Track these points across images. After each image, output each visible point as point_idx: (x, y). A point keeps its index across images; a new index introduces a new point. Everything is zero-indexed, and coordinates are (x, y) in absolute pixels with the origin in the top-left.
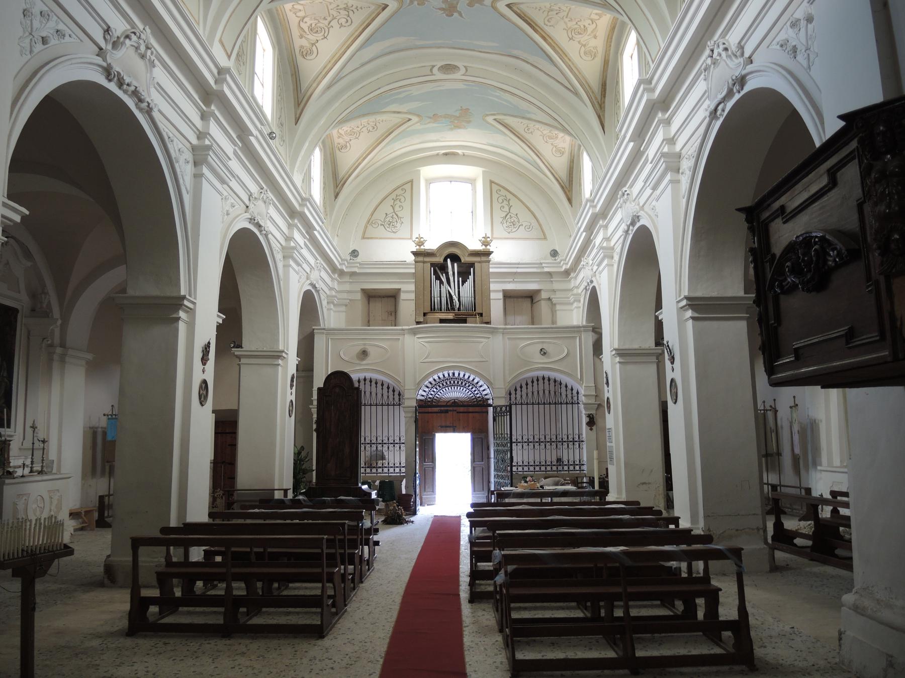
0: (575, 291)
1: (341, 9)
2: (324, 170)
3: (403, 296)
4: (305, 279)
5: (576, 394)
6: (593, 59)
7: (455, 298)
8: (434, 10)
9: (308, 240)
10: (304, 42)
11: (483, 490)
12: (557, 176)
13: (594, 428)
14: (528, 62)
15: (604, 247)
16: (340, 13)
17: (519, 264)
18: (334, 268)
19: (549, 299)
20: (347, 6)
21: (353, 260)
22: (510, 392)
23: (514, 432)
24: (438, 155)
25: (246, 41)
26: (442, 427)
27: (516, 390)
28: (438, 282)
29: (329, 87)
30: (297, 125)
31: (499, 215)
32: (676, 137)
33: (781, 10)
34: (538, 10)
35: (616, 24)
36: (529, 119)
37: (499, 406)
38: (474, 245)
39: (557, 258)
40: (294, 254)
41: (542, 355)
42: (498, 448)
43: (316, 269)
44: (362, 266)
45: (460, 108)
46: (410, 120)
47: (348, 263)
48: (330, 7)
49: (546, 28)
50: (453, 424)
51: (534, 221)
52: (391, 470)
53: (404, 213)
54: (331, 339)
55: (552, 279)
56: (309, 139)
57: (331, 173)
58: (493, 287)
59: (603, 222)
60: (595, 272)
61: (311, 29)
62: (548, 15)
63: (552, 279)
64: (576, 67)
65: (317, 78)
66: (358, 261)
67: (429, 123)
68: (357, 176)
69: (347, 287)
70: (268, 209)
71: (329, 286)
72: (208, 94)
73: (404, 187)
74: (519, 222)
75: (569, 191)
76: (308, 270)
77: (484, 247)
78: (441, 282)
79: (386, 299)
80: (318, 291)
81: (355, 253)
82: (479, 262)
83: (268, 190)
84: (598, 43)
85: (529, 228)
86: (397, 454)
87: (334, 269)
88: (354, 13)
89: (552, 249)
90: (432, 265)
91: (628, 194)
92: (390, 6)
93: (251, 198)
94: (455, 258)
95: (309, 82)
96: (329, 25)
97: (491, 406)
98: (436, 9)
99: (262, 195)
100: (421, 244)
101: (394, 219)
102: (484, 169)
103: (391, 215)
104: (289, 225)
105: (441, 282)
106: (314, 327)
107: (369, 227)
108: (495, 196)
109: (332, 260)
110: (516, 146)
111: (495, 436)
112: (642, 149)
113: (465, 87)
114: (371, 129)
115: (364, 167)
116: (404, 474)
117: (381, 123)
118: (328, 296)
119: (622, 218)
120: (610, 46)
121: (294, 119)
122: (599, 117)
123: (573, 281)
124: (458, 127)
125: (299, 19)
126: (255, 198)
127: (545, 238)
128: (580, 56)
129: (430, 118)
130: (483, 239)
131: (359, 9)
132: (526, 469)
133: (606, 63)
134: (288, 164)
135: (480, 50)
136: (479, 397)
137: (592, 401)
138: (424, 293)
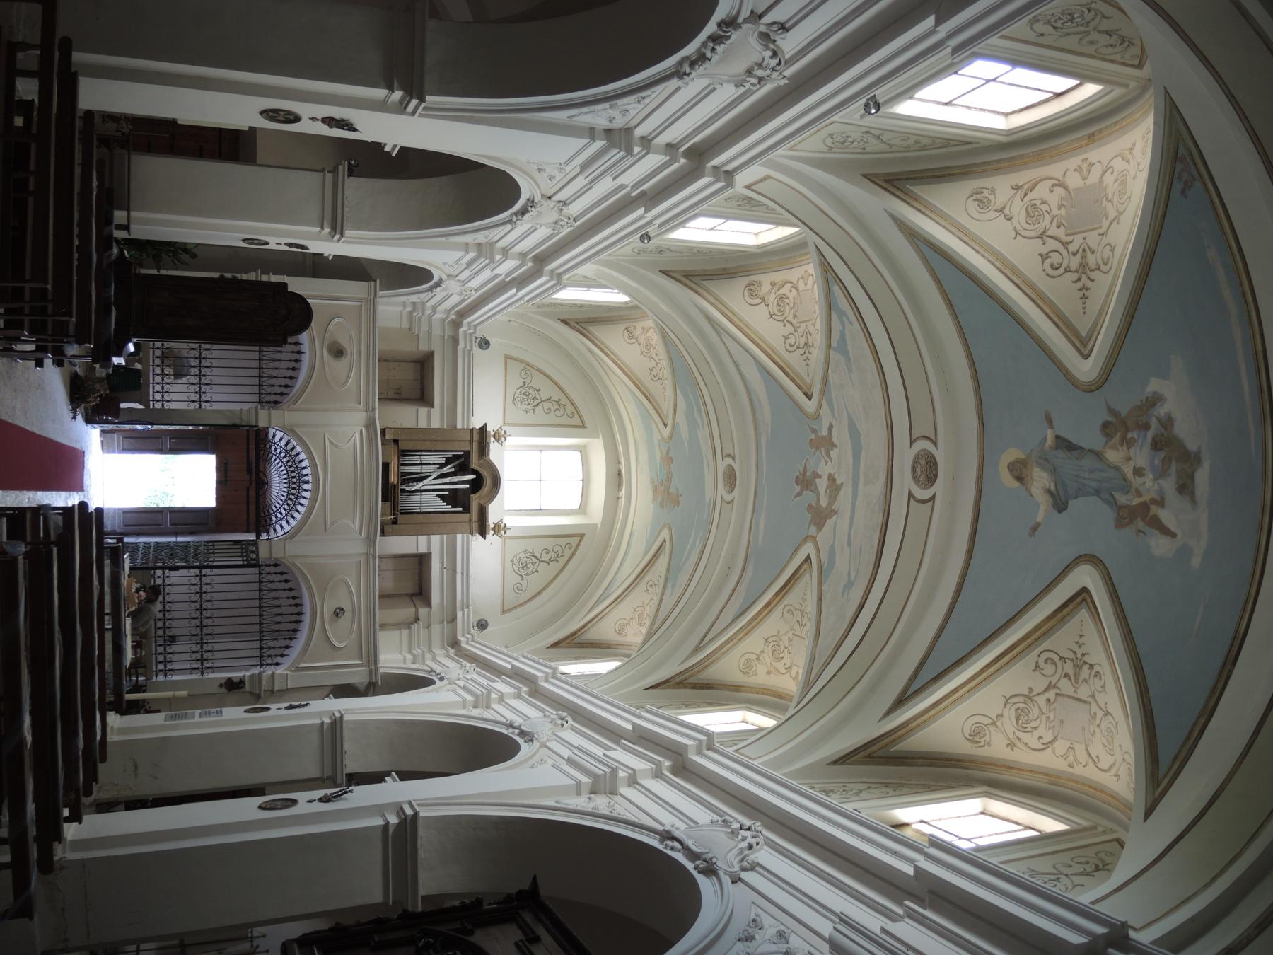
1: (807, 338)
2: (600, 306)
3: (423, 411)
7: (419, 486)
10: (766, 288)
12: (589, 626)
13: (224, 690)
14: (737, 584)
17: (468, 575)
19: (417, 620)
22: (279, 565)
27: (282, 573)
28: (443, 461)
29: (709, 318)
31: (537, 546)
32: (638, 787)
36: (664, 588)
37: (257, 548)
39: (476, 628)
47: (471, 334)
48: (809, 324)
51: (528, 595)
52: (158, 388)
58: (435, 539)
59: (525, 692)
62: (796, 610)
64: (730, 648)
65: (721, 303)
66: (474, 348)
67: (661, 452)
68: (590, 351)
69: (437, 331)
70: (546, 227)
73: (576, 415)
75: (569, 643)
76: (463, 277)
77: (492, 526)
78: (442, 466)
80: (431, 289)
81: (485, 344)
82: (471, 520)
85: (519, 589)
87: (463, 314)
90: (467, 454)
91: (562, 725)
94: (476, 485)
96: (788, 321)
99: (566, 220)
102: (599, 525)
103: (538, 397)
105: (442, 466)
106: (378, 281)
108: (563, 541)
110: (629, 570)
114: (654, 372)
119: (529, 718)
120: (758, 693)
122: (667, 681)
124: (655, 489)
125: (795, 283)
126: (562, 210)
127: (504, 612)
130: (503, 525)
133: (736, 688)
137: (265, 685)
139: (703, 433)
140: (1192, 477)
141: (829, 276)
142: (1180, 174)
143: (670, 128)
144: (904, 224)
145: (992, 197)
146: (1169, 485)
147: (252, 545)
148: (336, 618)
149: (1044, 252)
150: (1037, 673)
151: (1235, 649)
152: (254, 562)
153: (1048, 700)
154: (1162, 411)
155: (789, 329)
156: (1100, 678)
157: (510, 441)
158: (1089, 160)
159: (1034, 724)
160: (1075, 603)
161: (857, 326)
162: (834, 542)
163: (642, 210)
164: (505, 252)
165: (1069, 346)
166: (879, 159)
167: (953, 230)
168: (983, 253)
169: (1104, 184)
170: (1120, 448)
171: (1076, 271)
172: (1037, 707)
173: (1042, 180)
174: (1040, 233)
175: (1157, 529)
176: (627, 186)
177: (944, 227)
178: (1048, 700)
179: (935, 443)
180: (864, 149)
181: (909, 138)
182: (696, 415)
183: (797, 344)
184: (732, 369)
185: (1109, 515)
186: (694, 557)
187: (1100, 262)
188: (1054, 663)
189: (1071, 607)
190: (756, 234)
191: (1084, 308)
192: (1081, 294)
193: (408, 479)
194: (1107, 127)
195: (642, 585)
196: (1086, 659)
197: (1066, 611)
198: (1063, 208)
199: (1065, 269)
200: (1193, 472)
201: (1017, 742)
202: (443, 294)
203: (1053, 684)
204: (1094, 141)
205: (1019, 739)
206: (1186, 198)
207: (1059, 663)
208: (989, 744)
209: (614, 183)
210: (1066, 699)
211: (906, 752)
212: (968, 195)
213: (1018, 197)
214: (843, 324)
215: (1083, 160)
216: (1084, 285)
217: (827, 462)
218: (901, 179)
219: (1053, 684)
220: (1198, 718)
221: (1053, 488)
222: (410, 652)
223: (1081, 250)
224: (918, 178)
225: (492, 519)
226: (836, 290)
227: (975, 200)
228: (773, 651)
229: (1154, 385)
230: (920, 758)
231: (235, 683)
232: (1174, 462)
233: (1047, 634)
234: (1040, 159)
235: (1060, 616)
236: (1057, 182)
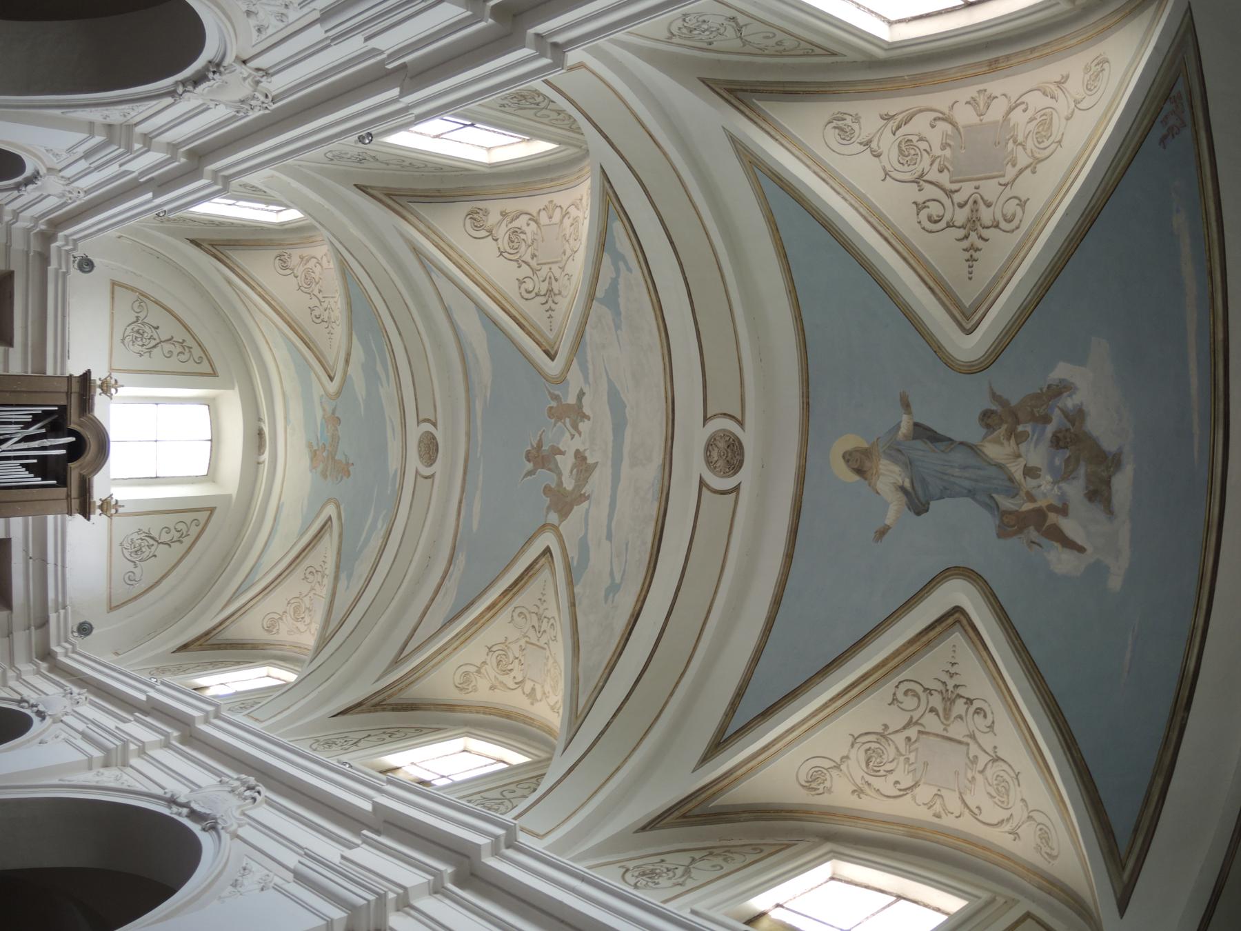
0: (11, 674)
1: (550, 283)
2: (244, 226)
4: (50, 165)
6: (457, 687)
8: (540, 433)
9: (136, 179)
10: (493, 218)
12: (227, 623)
14: (443, 578)
15: (128, 746)
16: (544, 281)
17: (63, 567)
18: (60, 223)
20: (555, 295)
21: (74, 262)
24: (260, 420)
25: (537, 119)
28: (29, 419)
29: (417, 251)
30: (355, 188)
31: (155, 525)
32: (413, 912)
34: (541, 596)
35: (515, 720)
36: (336, 578)
38: (100, 488)
39: (76, 634)
43: (68, 188)
44: (60, 275)
45: (351, 462)
46: (331, 379)
47: (67, 252)
48: (555, 267)
49: (510, 609)
53: (157, 359)
55: (33, 628)
56: (327, 205)
57: (238, 238)
58: (17, 523)
59: (175, 738)
60: (61, 721)
61: (516, 231)
62: (530, 613)
63: (33, 628)
64: (443, 659)
65: (434, 232)
66: (72, 270)
67: (324, 410)
68: (229, 282)
69: (18, 244)
70: (227, 106)
71: (22, 211)
72: (515, 16)
73: (205, 361)
74: (140, 561)
75: (200, 645)
76: (68, 173)
77: (99, 503)
78: (27, 425)
80: (17, 187)
81: (86, 265)
82: (68, 496)
83: (267, 112)
84: (482, 693)
85: (131, 579)
87: (57, 224)
88: (542, 304)
89: (94, 626)
90: (63, 410)
91: (254, 799)
92: (552, 364)
93: (261, 73)
94: (76, 450)
95: (427, 217)
96: (523, 261)
98: (541, 436)
99: (262, 98)
100: (105, 388)
102: (234, 496)
103: (155, 336)
104: (174, 145)
105: (27, 425)
108: (188, 517)
109: (78, 223)
110: (279, 551)
112: (365, 832)
113: (391, 472)
114: (317, 312)
115: (243, 292)
117: (327, 330)
119: (199, 787)
120: (478, 712)
121: (367, 184)
122: (360, 704)
123: (31, 667)
124: (314, 455)
125: (535, 214)
126: (258, 83)
127: (112, 608)
128: (461, 666)
129: (333, 413)
130: (113, 502)
131: (548, 314)
133: (450, 707)
135: (464, 501)
138: (7, 391)
139: (386, 391)
140: (1108, 483)
141: (612, 208)
142: (1166, 117)
144: (746, 148)
145: (856, 126)
146: (1075, 490)
149: (920, 201)
150: (894, 707)
151: (1185, 693)
153: (908, 739)
154: (1070, 402)
155: (526, 270)
156: (985, 716)
157: (123, 391)
158: (988, 93)
159: (889, 767)
160: (944, 625)
161: (637, 274)
162: (586, 533)
163: (395, 92)
164: (148, 140)
165: (947, 317)
166: (719, 61)
167: (809, 162)
168: (845, 194)
169: (1011, 124)
170: (1005, 442)
171: (963, 227)
172: (892, 747)
173: (921, 111)
174: (916, 175)
175: (1057, 541)
176: (382, 52)
177: (797, 157)
178: (908, 739)
179: (741, 423)
180: (710, 43)
181: (775, 35)
182: (379, 368)
183: (536, 290)
184: (441, 317)
185: (989, 522)
186: (376, 542)
187: (999, 217)
188: (916, 695)
189: (938, 629)
190: (489, 149)
191: (971, 273)
192: (967, 255)
194: (1017, 54)
195: (299, 572)
196: (960, 691)
197: (932, 634)
198: (948, 148)
199: (948, 223)
200: (1110, 477)
201: (866, 788)
202: (36, 194)
203: (914, 720)
204: (997, 69)
205: (869, 785)
206: (1165, 148)
207: (923, 696)
208: (829, 790)
209: (366, 44)
210: (932, 738)
211: (727, 806)
212: (826, 120)
213: (888, 132)
214: (617, 271)
215: (979, 92)
216: (972, 245)
217: (573, 437)
218: (746, 91)
219: (914, 720)
220: (1153, 778)
221: (907, 484)
223: (971, 201)
224: (766, 92)
225: (98, 495)
226: (617, 227)
227: (835, 128)
228: (499, 662)
229: (1062, 371)
230: (744, 812)
232: (1082, 463)
233: (908, 661)
234: (917, 85)
235: (925, 639)
236: (941, 115)
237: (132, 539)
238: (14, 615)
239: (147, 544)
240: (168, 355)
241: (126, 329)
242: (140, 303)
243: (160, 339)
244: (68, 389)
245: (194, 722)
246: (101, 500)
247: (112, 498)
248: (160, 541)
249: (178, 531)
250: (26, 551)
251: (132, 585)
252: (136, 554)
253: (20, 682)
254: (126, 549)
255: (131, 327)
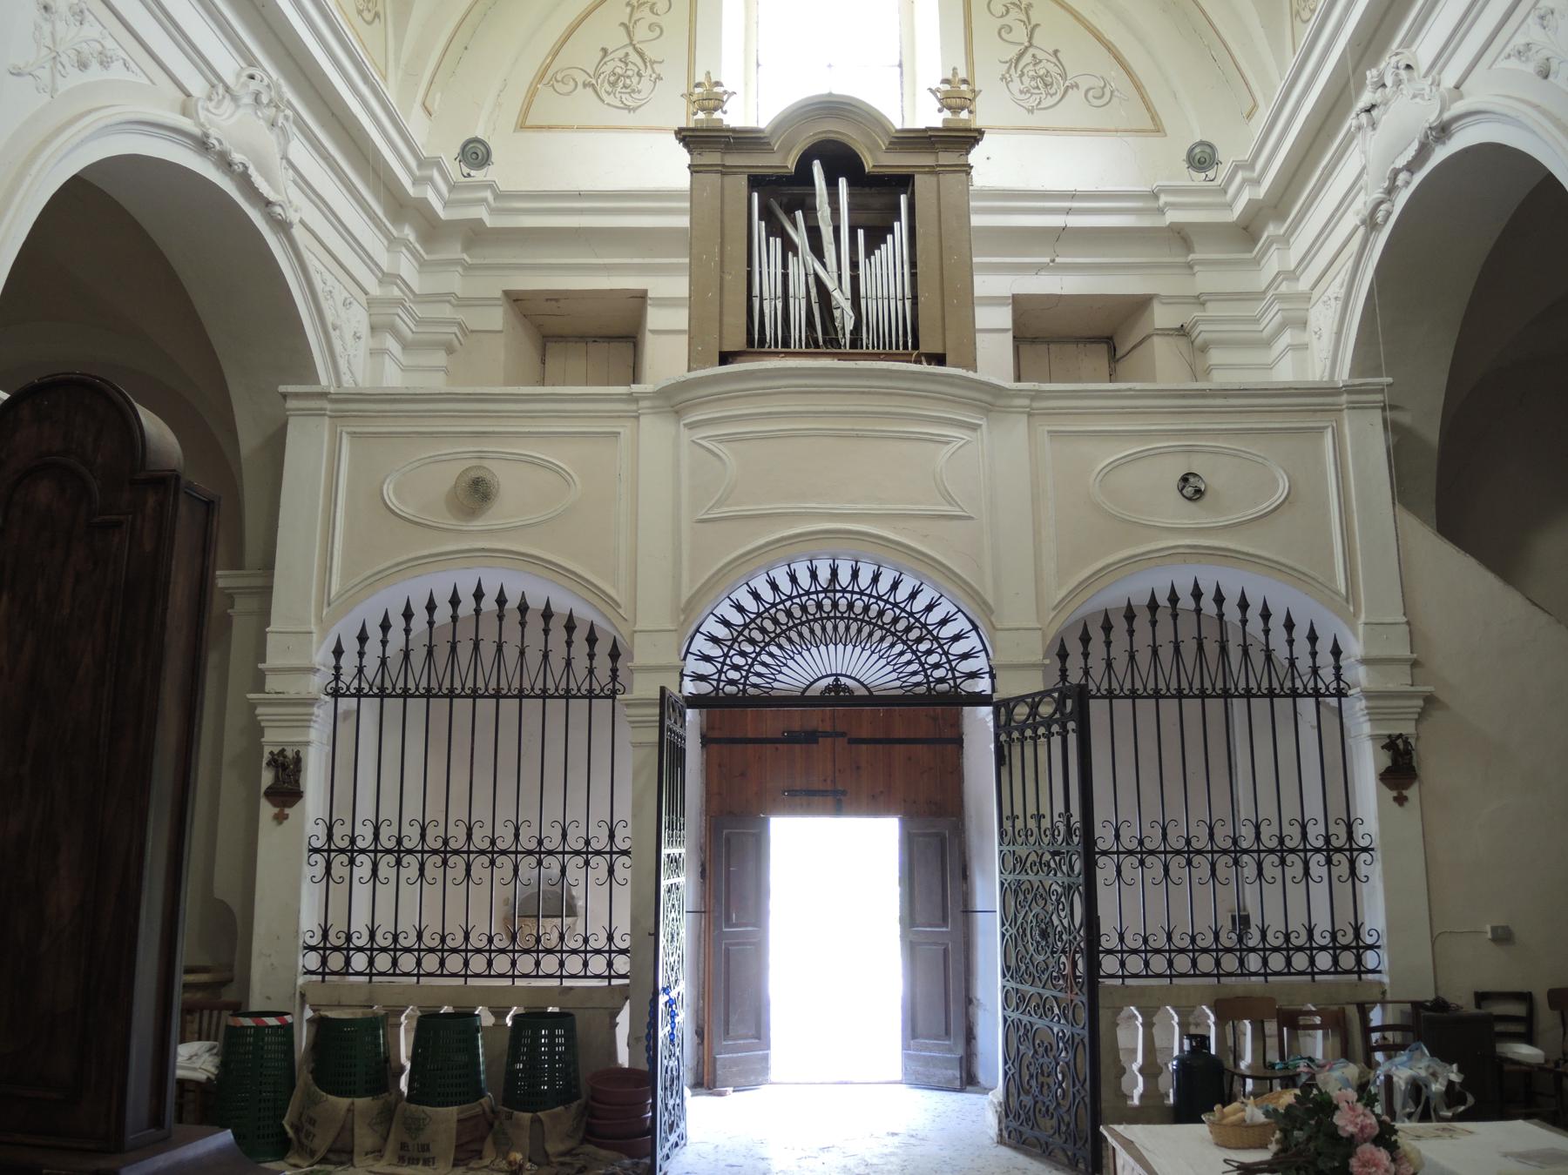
3: (655, 318)
5: (1331, 659)
7: (841, 298)
11: (947, 1032)
13: (1412, 793)
17: (1073, 196)
19: (1182, 332)
22: (1063, 646)
23: (1102, 811)
26: (793, 793)
27: (1085, 639)
28: (777, 242)
33: (1485, 38)
37: (1021, 699)
40: (398, 318)
41: (1190, 499)
42: (1023, 877)
50: (834, 782)
51: (1115, 74)
52: (574, 964)
54: (353, 434)
58: (984, 285)
63: (1191, 257)
78: (789, 246)
79: (603, 346)
81: (475, 154)
85: (1101, 95)
86: (1296, 892)
90: (757, 182)
94: (841, 161)
97: (979, 700)
101: (630, 66)
103: (621, 54)
105: (789, 246)
106: (282, 388)
107: (544, 91)
111: (1007, 825)
116: (627, 981)
118: (372, 302)
127: (1158, 129)
132: (1135, 964)
134: (391, 78)
136: (941, 680)
137: (1398, 680)
138: (722, 279)
143: (335, 209)
147: (1010, 713)
148: (1207, 499)
152: (1069, 703)
193: (825, 332)
222: (1268, 343)
225: (930, 116)
231: (1394, 761)
237: (1021, 92)
238: (1162, 293)
239: (1031, 67)
240: (658, 29)
241: (608, 104)
242: (557, 81)
243: (625, 46)
244: (717, 172)
245: (1257, 201)
246: (940, 111)
247: (938, 90)
248: (1027, 44)
249: (1008, 12)
250: (1038, 269)
251: (1112, 92)
252: (1052, 84)
253: (1301, 274)
254: (1039, 103)
255: (604, 96)
